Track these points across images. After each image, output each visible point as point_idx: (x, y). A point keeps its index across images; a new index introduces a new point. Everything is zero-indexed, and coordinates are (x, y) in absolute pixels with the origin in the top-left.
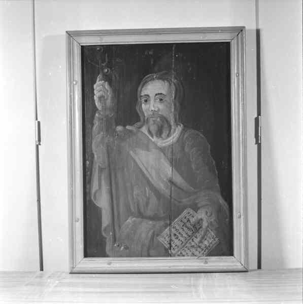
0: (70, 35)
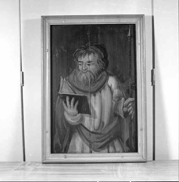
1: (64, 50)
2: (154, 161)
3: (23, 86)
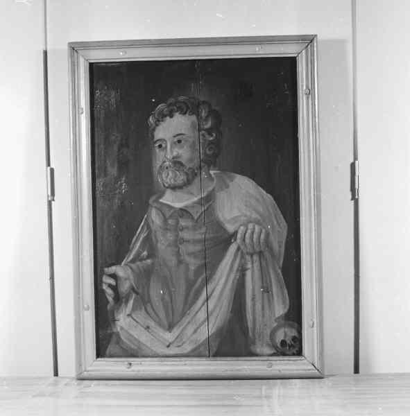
0: (74, 48)
1: (269, 104)
2: (356, 375)
3: (53, 200)
